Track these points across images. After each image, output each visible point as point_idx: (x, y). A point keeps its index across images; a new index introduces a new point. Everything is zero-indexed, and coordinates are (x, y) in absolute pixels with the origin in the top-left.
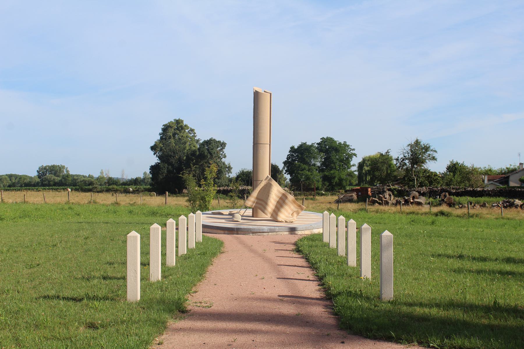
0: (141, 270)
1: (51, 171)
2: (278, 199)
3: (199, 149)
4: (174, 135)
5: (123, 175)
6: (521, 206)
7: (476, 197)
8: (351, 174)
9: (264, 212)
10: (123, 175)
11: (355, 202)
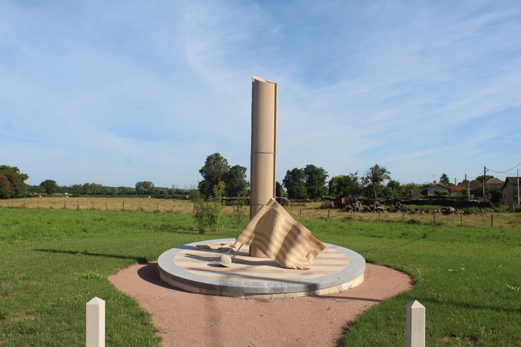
0: (98, 321)
1: (144, 185)
2: (286, 234)
4: (214, 163)
6: (455, 212)
8: (325, 188)
9: (265, 253)
11: (333, 208)
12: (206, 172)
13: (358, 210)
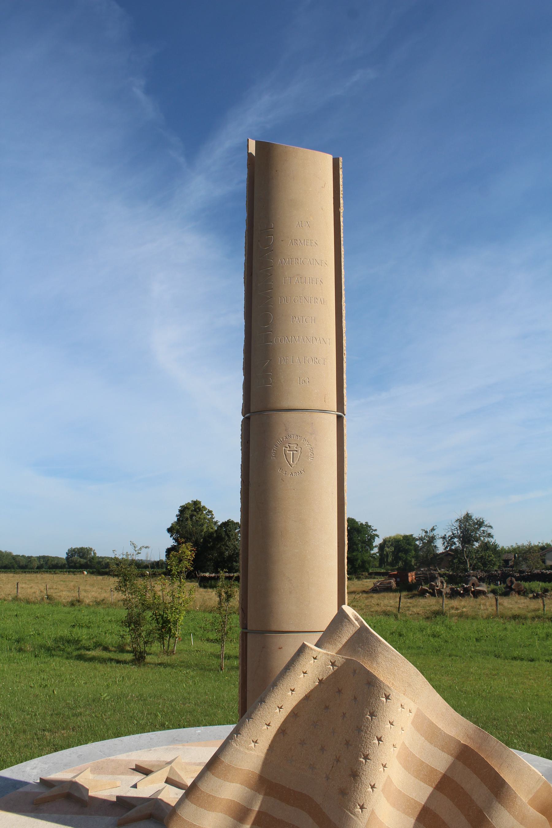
1: (79, 553)
2: (421, 793)
3: (216, 531)
4: (192, 516)
5: (147, 557)
8: (372, 556)
10: (147, 557)
11: (395, 591)
12: (178, 532)
13: (440, 593)
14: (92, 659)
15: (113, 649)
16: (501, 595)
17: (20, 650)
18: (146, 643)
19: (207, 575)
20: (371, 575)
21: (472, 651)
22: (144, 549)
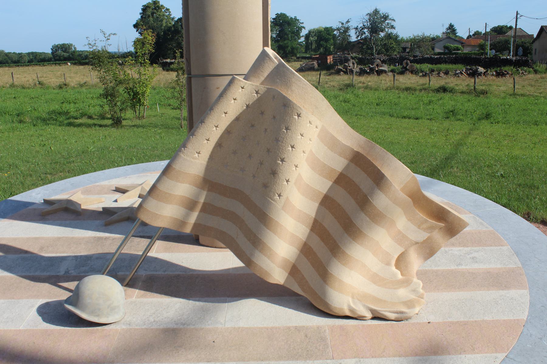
1: (62, 48)
2: (323, 186)
3: (174, 25)
4: (153, 14)
6: (485, 72)
7: (436, 64)
8: (300, 44)
11: (317, 70)
13: (352, 71)
14: (80, 125)
15: (96, 117)
16: (398, 74)
17: (21, 122)
18: (121, 110)
19: (168, 60)
20: (298, 59)
21: (373, 112)
22: (112, 36)
